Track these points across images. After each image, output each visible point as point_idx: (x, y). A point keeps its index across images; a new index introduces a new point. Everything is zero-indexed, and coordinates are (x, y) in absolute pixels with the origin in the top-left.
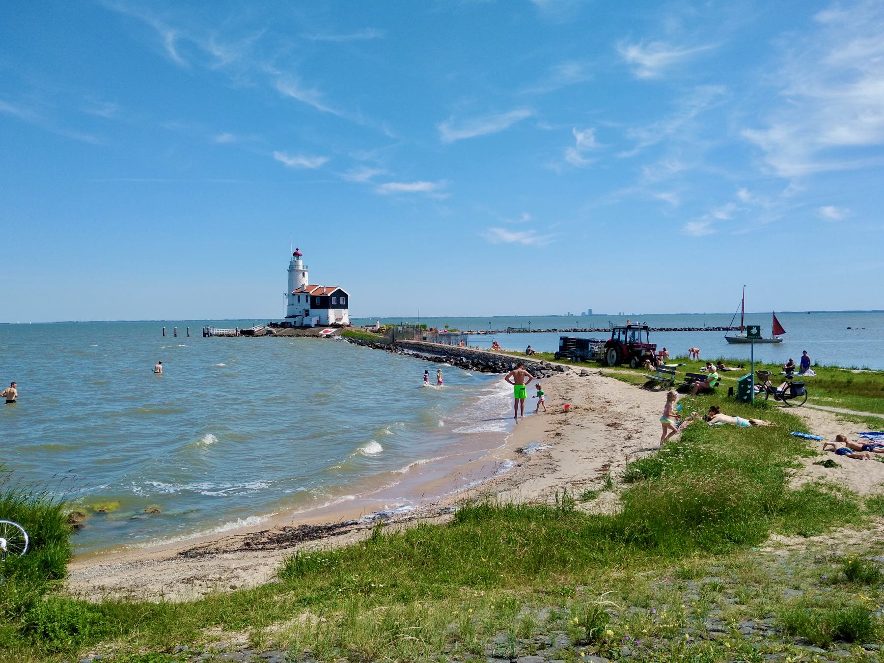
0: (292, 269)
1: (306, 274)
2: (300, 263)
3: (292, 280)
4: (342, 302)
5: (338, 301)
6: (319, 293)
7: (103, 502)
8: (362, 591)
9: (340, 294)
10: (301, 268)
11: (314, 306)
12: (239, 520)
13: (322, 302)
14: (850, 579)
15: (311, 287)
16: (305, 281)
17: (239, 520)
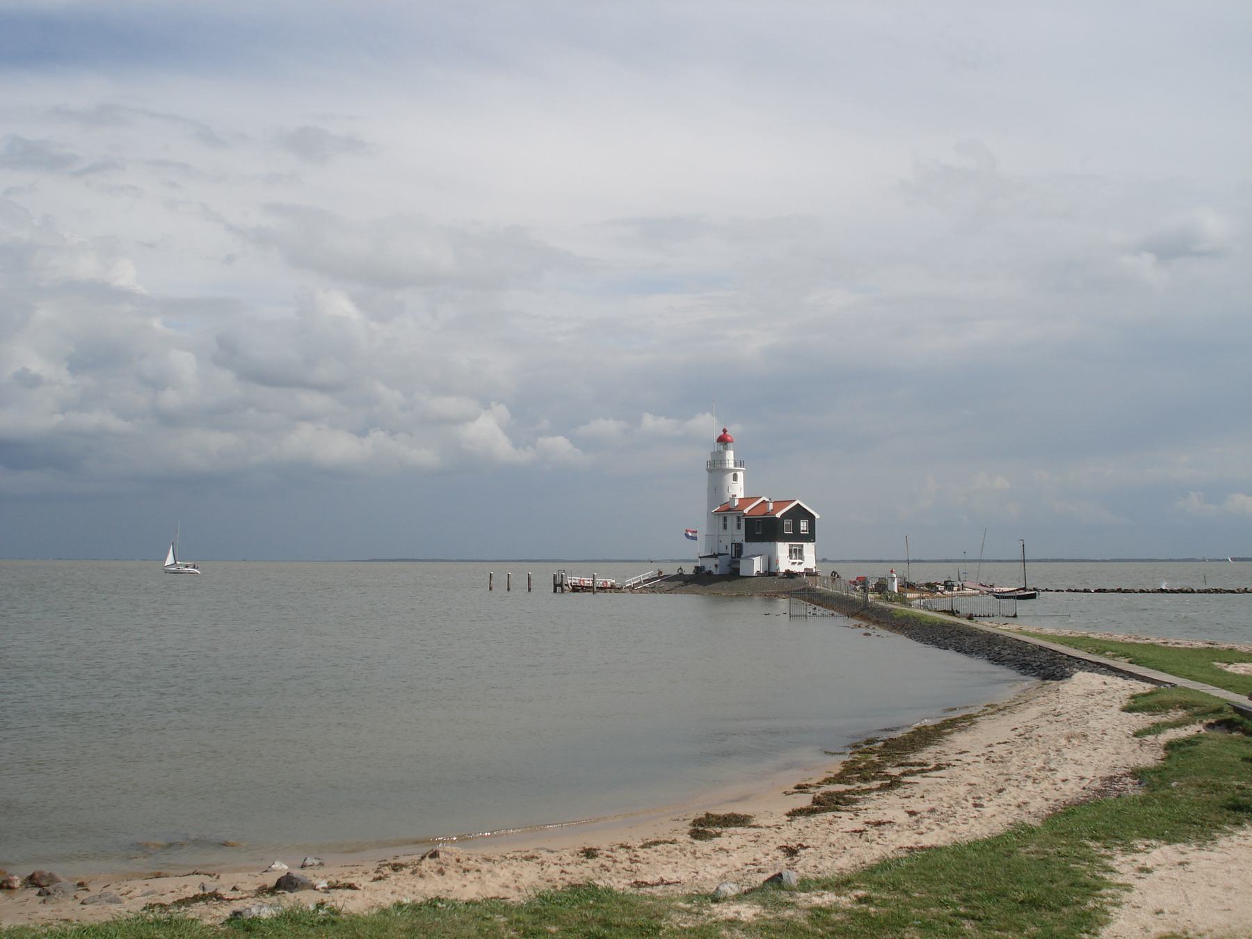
2: (730, 455)
4: (803, 525)
5: (796, 527)
9: (799, 513)
10: (731, 465)
11: (751, 537)
13: (764, 528)
16: (737, 490)
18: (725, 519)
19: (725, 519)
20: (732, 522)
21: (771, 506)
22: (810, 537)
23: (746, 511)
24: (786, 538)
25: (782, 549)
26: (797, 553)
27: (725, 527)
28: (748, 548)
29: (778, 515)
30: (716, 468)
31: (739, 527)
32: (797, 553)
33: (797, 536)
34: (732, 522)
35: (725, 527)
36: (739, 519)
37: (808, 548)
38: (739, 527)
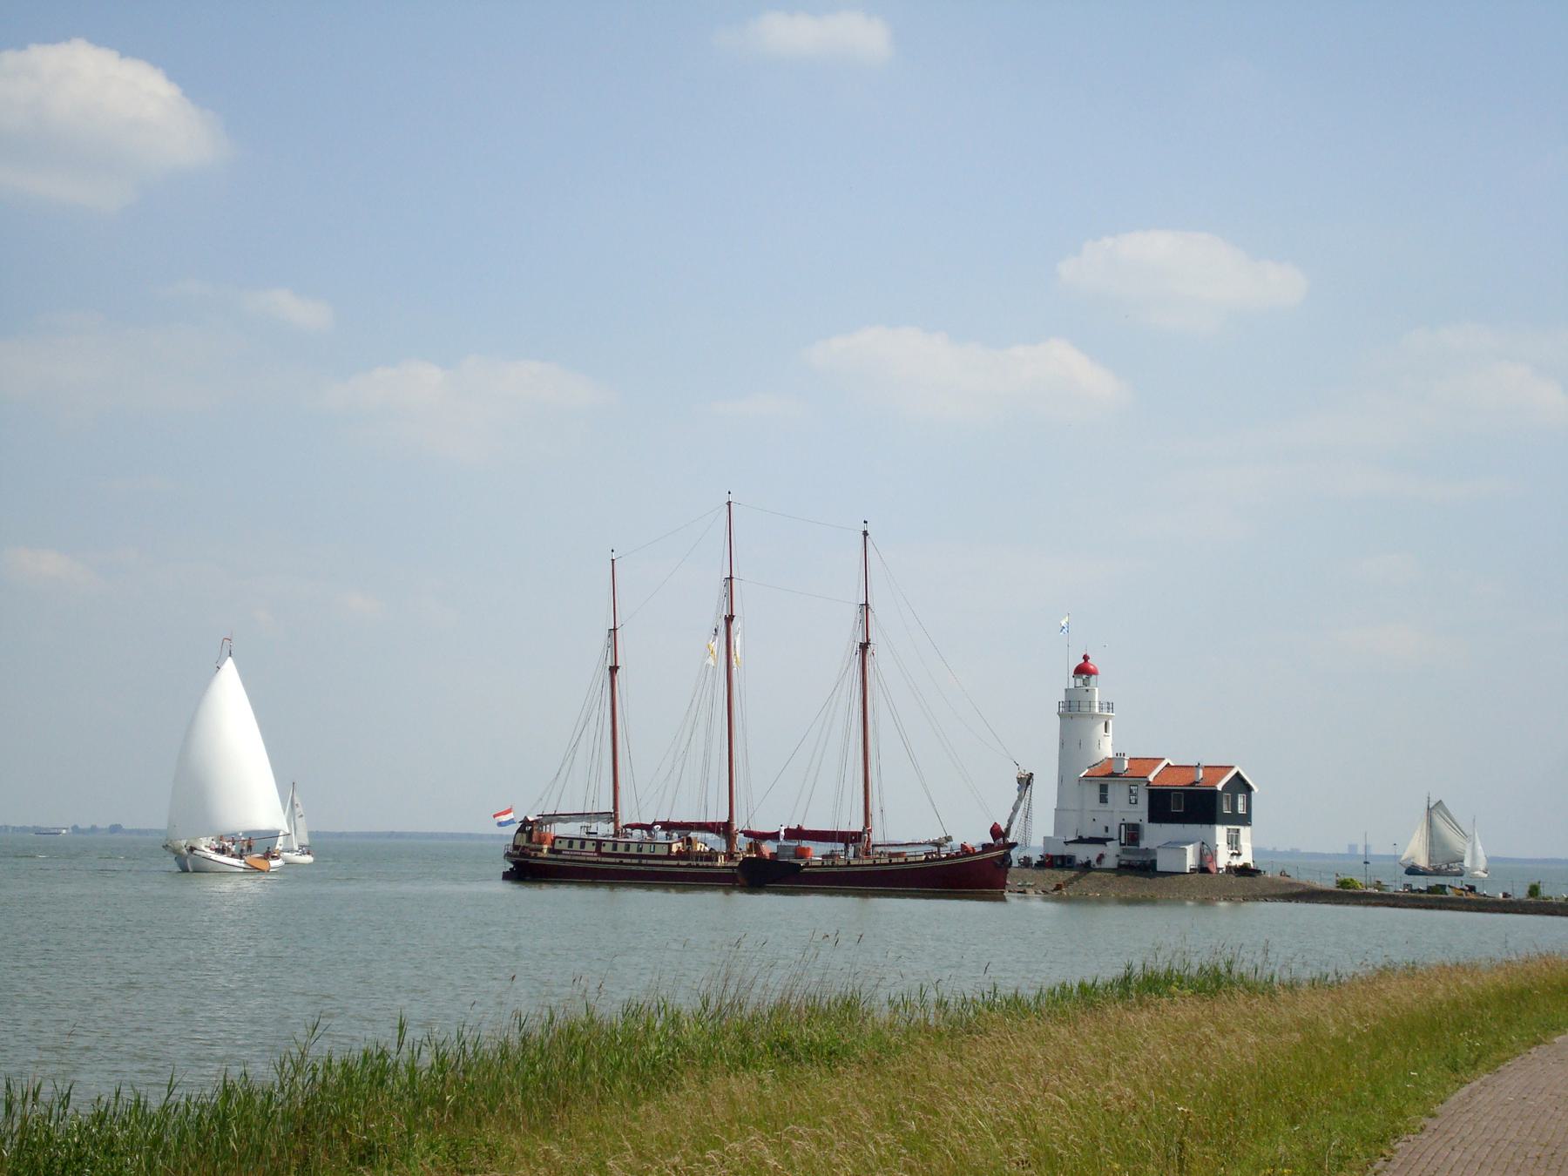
0: (1074, 710)
9: (1240, 785)
15: (1119, 757)
16: (1106, 747)
18: (1104, 788)
19: (1104, 788)
22: (1246, 820)
23: (1151, 778)
24: (1226, 820)
25: (1221, 832)
26: (1233, 841)
27: (1103, 799)
29: (1219, 787)
32: (1233, 841)
34: (1117, 792)
35: (1103, 799)
37: (1245, 832)
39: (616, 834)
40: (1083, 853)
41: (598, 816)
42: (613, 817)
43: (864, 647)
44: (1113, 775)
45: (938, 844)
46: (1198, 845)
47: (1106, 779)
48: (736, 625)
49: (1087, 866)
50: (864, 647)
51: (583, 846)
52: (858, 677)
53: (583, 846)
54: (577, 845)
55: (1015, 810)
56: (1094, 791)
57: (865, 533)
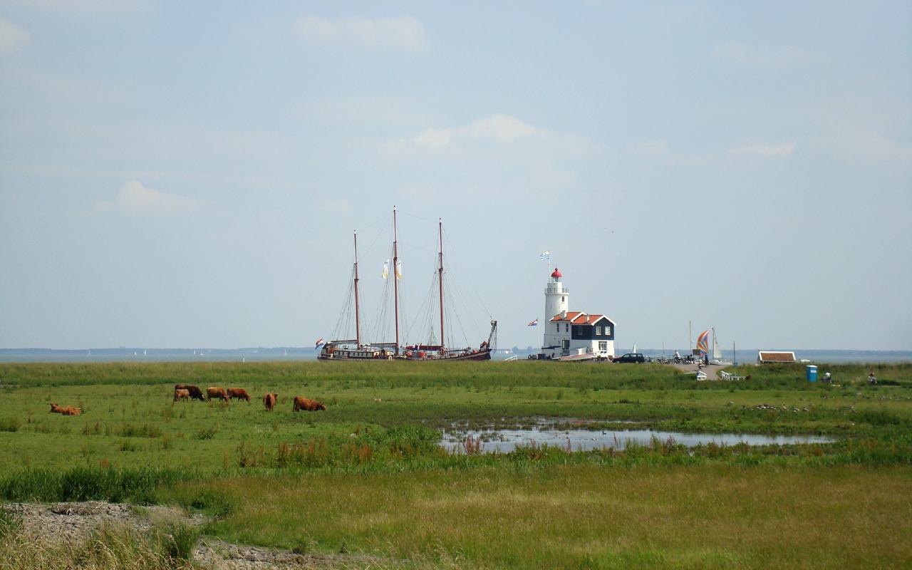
0: (550, 292)
1: (566, 298)
2: (560, 285)
3: (549, 306)
4: (607, 332)
5: (603, 331)
6: (580, 322)
7: (273, 384)
8: (58, 454)
9: (605, 323)
10: (560, 291)
11: (575, 336)
12: (768, 445)
13: (584, 331)
14: (768, 386)
15: (571, 314)
16: (563, 307)
17: (768, 445)
18: (558, 325)
19: (558, 325)
20: (563, 327)
21: (588, 319)
22: (611, 337)
23: (572, 321)
25: (595, 344)
28: (573, 343)
29: (593, 324)
30: (550, 292)
31: (567, 330)
32: (604, 346)
33: (603, 337)
36: (567, 325)
37: (610, 343)
38: (567, 330)
39: (359, 349)
40: (548, 353)
41: (350, 342)
42: (357, 342)
43: (441, 270)
44: (561, 320)
45: (466, 350)
46: (585, 348)
47: (559, 321)
48: (399, 261)
49: (549, 358)
50: (441, 270)
51: (343, 354)
52: (359, 310)
53: (343, 354)
54: (342, 353)
55: (491, 336)
56: (555, 325)
57: (440, 224)
